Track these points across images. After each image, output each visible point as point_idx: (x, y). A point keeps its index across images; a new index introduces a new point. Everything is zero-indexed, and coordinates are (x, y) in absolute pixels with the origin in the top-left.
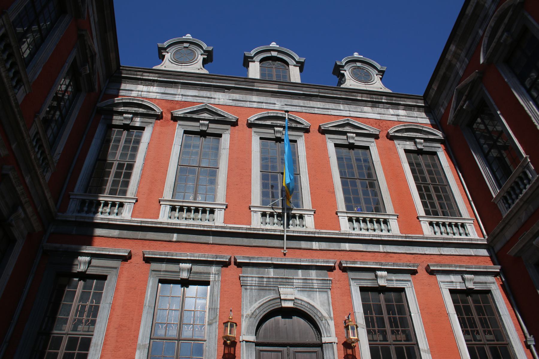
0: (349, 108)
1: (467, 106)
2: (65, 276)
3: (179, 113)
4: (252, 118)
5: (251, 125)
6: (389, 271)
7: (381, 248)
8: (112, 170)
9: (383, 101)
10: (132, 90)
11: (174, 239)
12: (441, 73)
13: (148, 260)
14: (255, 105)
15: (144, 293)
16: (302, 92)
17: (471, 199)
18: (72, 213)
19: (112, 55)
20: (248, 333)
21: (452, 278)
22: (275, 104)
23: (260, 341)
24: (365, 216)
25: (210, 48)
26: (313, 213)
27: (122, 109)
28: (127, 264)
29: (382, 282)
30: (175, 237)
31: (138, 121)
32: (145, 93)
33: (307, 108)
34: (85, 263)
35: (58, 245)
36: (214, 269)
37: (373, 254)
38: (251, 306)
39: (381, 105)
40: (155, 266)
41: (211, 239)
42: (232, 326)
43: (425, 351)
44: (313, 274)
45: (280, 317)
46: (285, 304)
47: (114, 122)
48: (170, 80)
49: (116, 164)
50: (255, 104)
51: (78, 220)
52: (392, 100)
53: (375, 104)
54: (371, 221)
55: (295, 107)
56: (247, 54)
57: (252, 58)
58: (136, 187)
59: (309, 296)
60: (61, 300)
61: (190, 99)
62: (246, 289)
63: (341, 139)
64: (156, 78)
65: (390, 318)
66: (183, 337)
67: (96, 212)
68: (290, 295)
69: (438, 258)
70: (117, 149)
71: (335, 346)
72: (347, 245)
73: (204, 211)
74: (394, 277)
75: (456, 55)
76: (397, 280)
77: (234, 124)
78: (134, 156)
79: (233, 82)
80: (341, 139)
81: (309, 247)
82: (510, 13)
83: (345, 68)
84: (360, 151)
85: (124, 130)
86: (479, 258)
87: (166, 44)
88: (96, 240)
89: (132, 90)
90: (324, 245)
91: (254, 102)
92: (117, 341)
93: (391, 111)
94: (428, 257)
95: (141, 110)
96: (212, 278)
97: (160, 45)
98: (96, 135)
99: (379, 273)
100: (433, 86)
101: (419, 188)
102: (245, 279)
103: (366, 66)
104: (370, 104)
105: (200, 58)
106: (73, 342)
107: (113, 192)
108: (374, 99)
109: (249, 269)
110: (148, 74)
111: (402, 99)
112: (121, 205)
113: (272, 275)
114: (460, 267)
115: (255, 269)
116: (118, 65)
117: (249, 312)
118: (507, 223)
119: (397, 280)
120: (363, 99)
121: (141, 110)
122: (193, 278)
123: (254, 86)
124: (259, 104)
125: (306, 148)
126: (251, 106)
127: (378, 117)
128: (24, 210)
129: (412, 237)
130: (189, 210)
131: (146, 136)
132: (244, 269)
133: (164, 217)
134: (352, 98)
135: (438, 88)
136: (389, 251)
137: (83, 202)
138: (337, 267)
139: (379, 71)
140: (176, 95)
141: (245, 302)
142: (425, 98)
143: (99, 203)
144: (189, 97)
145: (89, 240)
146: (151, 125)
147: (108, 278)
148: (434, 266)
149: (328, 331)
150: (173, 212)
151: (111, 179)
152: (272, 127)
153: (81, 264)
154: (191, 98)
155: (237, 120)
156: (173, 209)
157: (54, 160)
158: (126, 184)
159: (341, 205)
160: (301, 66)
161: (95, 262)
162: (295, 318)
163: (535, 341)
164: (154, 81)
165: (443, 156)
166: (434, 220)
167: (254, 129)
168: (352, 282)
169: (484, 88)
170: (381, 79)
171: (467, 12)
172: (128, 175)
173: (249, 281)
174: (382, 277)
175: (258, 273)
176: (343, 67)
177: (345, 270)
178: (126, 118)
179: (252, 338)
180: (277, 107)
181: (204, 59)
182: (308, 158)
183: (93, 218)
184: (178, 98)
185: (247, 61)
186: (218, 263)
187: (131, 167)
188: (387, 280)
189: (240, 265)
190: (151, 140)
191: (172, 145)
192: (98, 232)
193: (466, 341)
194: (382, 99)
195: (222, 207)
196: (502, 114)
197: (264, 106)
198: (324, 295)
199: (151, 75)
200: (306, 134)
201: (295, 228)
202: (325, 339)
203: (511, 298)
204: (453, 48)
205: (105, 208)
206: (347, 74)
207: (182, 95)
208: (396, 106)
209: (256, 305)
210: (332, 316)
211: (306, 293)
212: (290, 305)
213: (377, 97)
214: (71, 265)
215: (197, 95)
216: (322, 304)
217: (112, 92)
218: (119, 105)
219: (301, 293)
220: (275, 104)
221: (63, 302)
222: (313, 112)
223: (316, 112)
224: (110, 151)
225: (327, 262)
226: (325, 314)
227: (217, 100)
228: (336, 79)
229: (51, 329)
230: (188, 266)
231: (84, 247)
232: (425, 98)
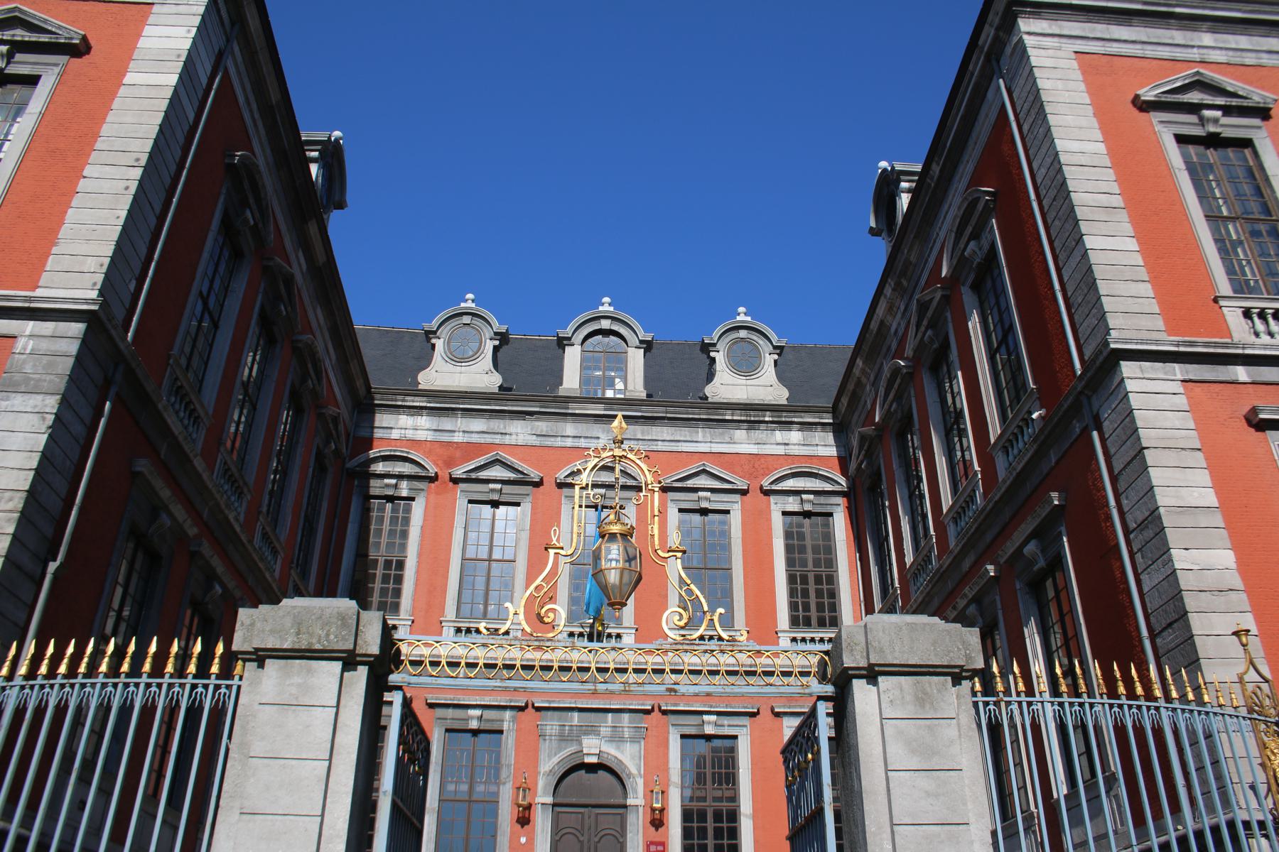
6: (719, 714)
14: (569, 443)
20: (545, 794)
23: (559, 800)
28: (76, 62)
29: (709, 730)
36: (508, 714)
38: (550, 762)
39: (763, 426)
40: (440, 712)
42: (524, 790)
43: (746, 816)
46: (588, 760)
47: (373, 492)
48: (447, 403)
49: (381, 560)
59: (618, 748)
65: (714, 774)
66: (475, 797)
68: (592, 748)
71: (641, 809)
87: (434, 324)
96: (505, 726)
101: (791, 579)
103: (755, 337)
108: (753, 415)
113: (576, 722)
115: (557, 713)
116: (369, 388)
122: (485, 726)
126: (563, 444)
128: (171, 515)
131: (418, 509)
134: (720, 416)
141: (543, 756)
149: (635, 791)
156: (458, 630)
166: (799, 636)
172: (399, 579)
173: (548, 730)
174: (709, 723)
179: (549, 800)
186: (512, 708)
198: (636, 746)
208: (786, 425)
209: (556, 760)
212: (594, 760)
216: (632, 758)
218: (376, 460)
223: (659, 448)
224: (371, 540)
226: (634, 770)
232: (834, 410)
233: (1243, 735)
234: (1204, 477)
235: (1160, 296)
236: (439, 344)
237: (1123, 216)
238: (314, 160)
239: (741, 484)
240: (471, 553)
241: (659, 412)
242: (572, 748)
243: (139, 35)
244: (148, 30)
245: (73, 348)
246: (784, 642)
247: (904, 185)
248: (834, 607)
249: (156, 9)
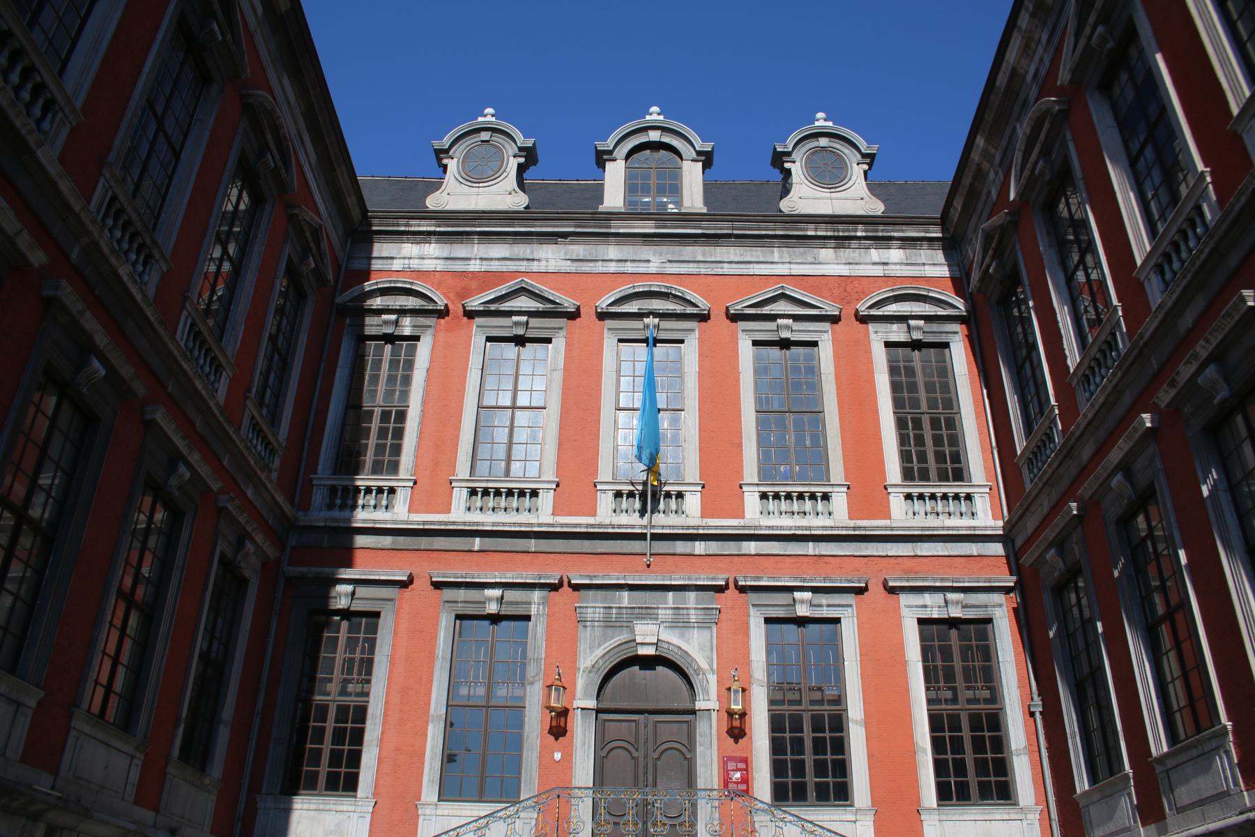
0: (790, 256)
1: (995, 270)
2: (320, 617)
3: (475, 303)
4: (603, 303)
5: (602, 316)
6: (815, 590)
7: (811, 548)
8: (373, 426)
9: (859, 234)
10: (392, 258)
11: (476, 548)
12: (967, 181)
13: (438, 586)
14: (612, 267)
15: (434, 638)
16: (699, 231)
17: (994, 444)
18: (319, 515)
19: (351, 201)
20: (586, 696)
21: (927, 598)
22: (649, 261)
24: (789, 489)
25: (529, 143)
26: (699, 488)
27: (378, 302)
28: (407, 593)
30: (477, 543)
31: (407, 326)
32: (417, 261)
33: (708, 265)
34: (346, 595)
35: (305, 569)
36: (537, 595)
37: (795, 559)
38: (592, 654)
39: (854, 243)
40: (448, 594)
41: (532, 544)
43: (856, 722)
44: (692, 595)
45: (637, 668)
46: (643, 651)
47: (369, 331)
48: (460, 227)
49: (378, 411)
50: (614, 264)
51: (329, 524)
52: (877, 231)
53: (841, 242)
54: (801, 496)
55: (686, 265)
56: (601, 146)
57: (611, 152)
58: (412, 458)
59: (682, 636)
60: (318, 651)
61: (495, 266)
62: (585, 626)
63: (765, 330)
64: (432, 229)
67: (354, 507)
68: (648, 636)
69: (909, 563)
70: (378, 382)
71: (714, 714)
72: (753, 544)
73: (522, 493)
74: (824, 599)
75: (985, 154)
76: (829, 606)
77: (574, 315)
78: (405, 395)
79: (572, 223)
80: (765, 330)
81: (688, 551)
82: (1046, 126)
83: (794, 156)
84: (801, 350)
85: (342, 620)
86: (985, 560)
87: (446, 142)
88: (359, 556)
89: (392, 258)
90: (714, 547)
91: (611, 260)
92: (401, 711)
93: (875, 254)
94: (892, 561)
95: (411, 302)
97: (437, 144)
98: (341, 362)
99: (797, 595)
100: (955, 203)
101: (901, 424)
102: (584, 611)
103: (838, 145)
104: (832, 243)
105: (513, 164)
106: (343, 711)
107: (377, 469)
108: (840, 231)
109: (591, 593)
110: (417, 222)
111: (897, 227)
112: (392, 491)
114: (942, 580)
115: (600, 593)
116: (364, 211)
117: (589, 663)
118: (1027, 509)
119: (829, 606)
120: (819, 233)
121: (411, 302)
123: (610, 227)
124: (620, 264)
125: (700, 355)
126: (605, 270)
127: (844, 270)
129: (865, 528)
130: (498, 493)
131: (424, 351)
132: (583, 593)
133: (459, 513)
135: (963, 207)
136: (824, 553)
137: (333, 490)
138: (732, 585)
139: (864, 156)
140: (469, 259)
141: (583, 647)
142: (944, 221)
143: (357, 490)
144: (493, 263)
145: (346, 557)
146: (430, 331)
147: (382, 615)
148: (895, 580)
150: (474, 498)
151: (372, 441)
152: (639, 316)
153: (341, 596)
154: (497, 263)
155: (578, 308)
156: (473, 492)
157: (281, 439)
158: (397, 450)
159: (750, 471)
160: (707, 159)
161: (362, 591)
162: (660, 669)
163: (1043, 706)
164: (429, 233)
165: (960, 356)
166: (915, 491)
167: (609, 323)
168: (752, 611)
169: (1018, 247)
170: (865, 173)
171: (998, 83)
174: (802, 602)
175: (604, 600)
176: (789, 154)
177: (743, 590)
178: (386, 323)
179: (592, 703)
180: (653, 268)
181: (520, 165)
182: (700, 375)
183: (349, 520)
184: (475, 266)
185: (602, 158)
187: (402, 416)
188: (811, 605)
189: (576, 588)
190: (431, 362)
191: (466, 370)
192: (360, 541)
193: (929, 702)
194: (856, 231)
195: (549, 486)
196: (1035, 308)
197: (629, 267)
198: (706, 633)
199: (423, 222)
200: (703, 324)
201: (664, 521)
202: (699, 705)
203: (1025, 633)
204: (980, 141)
205: (368, 497)
206: (797, 169)
207: (481, 259)
209: (600, 652)
210: (715, 667)
211: (677, 631)
212: (650, 651)
213: (845, 227)
214: (326, 597)
215: (507, 255)
216: (702, 649)
217: (358, 265)
219: (670, 631)
220: (649, 261)
221: (322, 655)
222: (720, 271)
223: (726, 271)
225: (713, 579)
226: (704, 664)
227: (543, 263)
228: (777, 176)
229: (311, 692)
230: (497, 593)
231: (342, 570)
232: (944, 221)
236: (452, 165)
240: (489, 400)
242: (623, 637)
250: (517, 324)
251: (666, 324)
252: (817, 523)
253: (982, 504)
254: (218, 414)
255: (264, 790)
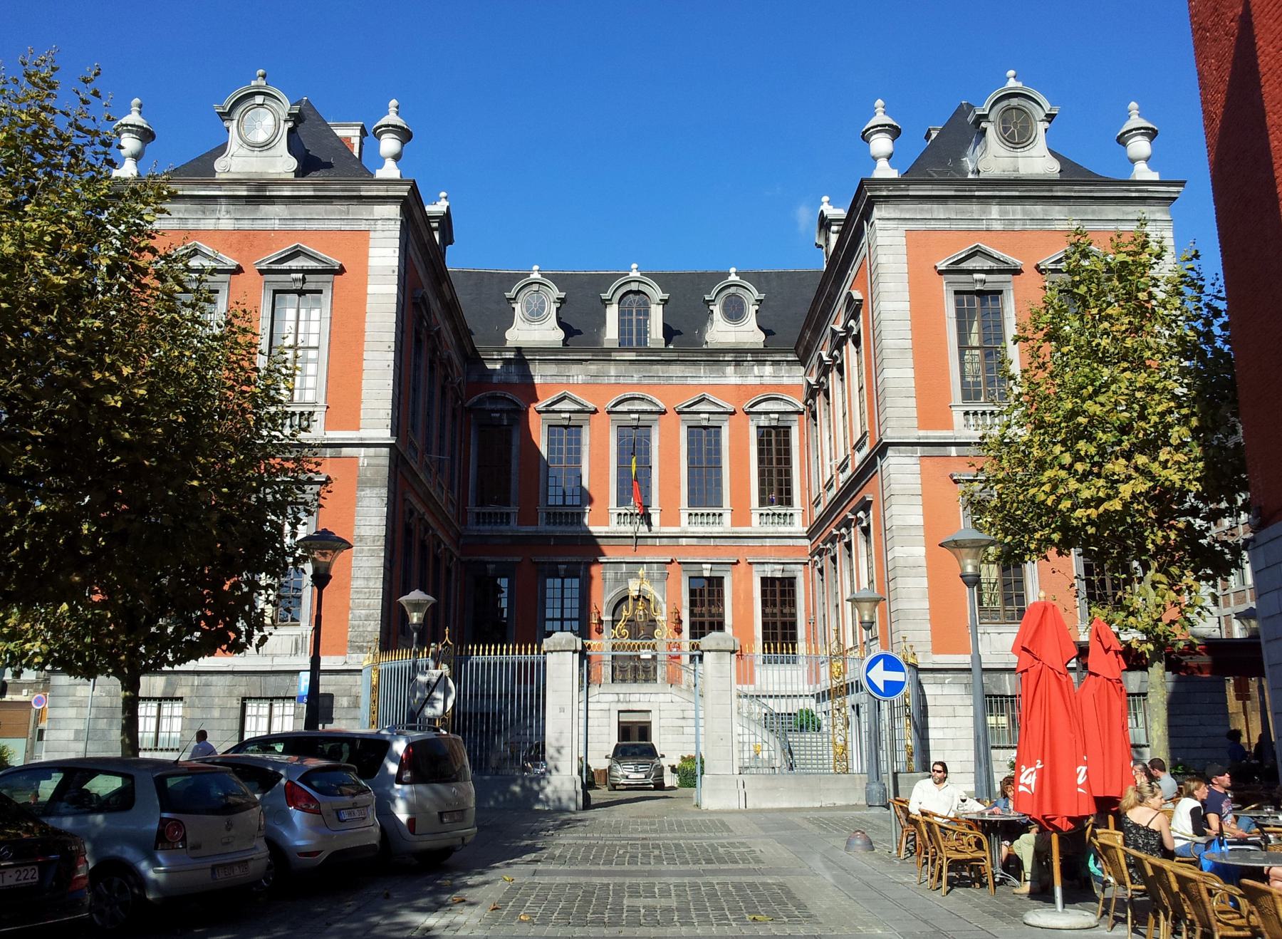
7: (712, 542)
14: (613, 380)
68: (633, 588)
108: (740, 356)
112: (720, 515)
133: (542, 527)
134: (716, 357)
137: (478, 514)
167: (612, 416)
180: (635, 380)
208: (762, 363)
209: (613, 594)
233: (980, 589)
234: (920, 510)
235: (919, 407)
236: (517, 307)
237: (910, 354)
238: (436, 229)
239: (730, 408)
241: (673, 356)
243: (367, 256)
244: (372, 252)
245: (386, 462)
246: (755, 518)
247: (834, 228)
248: (789, 492)
249: (372, 234)
250: (295, 280)
251: (643, 417)
252: (715, 530)
253: (798, 519)
254: (1248, 567)
255: (165, 815)
